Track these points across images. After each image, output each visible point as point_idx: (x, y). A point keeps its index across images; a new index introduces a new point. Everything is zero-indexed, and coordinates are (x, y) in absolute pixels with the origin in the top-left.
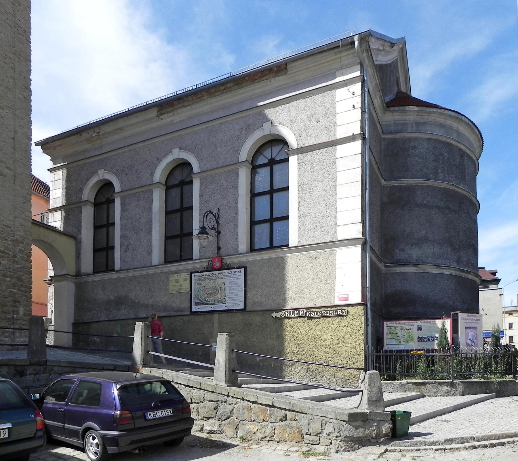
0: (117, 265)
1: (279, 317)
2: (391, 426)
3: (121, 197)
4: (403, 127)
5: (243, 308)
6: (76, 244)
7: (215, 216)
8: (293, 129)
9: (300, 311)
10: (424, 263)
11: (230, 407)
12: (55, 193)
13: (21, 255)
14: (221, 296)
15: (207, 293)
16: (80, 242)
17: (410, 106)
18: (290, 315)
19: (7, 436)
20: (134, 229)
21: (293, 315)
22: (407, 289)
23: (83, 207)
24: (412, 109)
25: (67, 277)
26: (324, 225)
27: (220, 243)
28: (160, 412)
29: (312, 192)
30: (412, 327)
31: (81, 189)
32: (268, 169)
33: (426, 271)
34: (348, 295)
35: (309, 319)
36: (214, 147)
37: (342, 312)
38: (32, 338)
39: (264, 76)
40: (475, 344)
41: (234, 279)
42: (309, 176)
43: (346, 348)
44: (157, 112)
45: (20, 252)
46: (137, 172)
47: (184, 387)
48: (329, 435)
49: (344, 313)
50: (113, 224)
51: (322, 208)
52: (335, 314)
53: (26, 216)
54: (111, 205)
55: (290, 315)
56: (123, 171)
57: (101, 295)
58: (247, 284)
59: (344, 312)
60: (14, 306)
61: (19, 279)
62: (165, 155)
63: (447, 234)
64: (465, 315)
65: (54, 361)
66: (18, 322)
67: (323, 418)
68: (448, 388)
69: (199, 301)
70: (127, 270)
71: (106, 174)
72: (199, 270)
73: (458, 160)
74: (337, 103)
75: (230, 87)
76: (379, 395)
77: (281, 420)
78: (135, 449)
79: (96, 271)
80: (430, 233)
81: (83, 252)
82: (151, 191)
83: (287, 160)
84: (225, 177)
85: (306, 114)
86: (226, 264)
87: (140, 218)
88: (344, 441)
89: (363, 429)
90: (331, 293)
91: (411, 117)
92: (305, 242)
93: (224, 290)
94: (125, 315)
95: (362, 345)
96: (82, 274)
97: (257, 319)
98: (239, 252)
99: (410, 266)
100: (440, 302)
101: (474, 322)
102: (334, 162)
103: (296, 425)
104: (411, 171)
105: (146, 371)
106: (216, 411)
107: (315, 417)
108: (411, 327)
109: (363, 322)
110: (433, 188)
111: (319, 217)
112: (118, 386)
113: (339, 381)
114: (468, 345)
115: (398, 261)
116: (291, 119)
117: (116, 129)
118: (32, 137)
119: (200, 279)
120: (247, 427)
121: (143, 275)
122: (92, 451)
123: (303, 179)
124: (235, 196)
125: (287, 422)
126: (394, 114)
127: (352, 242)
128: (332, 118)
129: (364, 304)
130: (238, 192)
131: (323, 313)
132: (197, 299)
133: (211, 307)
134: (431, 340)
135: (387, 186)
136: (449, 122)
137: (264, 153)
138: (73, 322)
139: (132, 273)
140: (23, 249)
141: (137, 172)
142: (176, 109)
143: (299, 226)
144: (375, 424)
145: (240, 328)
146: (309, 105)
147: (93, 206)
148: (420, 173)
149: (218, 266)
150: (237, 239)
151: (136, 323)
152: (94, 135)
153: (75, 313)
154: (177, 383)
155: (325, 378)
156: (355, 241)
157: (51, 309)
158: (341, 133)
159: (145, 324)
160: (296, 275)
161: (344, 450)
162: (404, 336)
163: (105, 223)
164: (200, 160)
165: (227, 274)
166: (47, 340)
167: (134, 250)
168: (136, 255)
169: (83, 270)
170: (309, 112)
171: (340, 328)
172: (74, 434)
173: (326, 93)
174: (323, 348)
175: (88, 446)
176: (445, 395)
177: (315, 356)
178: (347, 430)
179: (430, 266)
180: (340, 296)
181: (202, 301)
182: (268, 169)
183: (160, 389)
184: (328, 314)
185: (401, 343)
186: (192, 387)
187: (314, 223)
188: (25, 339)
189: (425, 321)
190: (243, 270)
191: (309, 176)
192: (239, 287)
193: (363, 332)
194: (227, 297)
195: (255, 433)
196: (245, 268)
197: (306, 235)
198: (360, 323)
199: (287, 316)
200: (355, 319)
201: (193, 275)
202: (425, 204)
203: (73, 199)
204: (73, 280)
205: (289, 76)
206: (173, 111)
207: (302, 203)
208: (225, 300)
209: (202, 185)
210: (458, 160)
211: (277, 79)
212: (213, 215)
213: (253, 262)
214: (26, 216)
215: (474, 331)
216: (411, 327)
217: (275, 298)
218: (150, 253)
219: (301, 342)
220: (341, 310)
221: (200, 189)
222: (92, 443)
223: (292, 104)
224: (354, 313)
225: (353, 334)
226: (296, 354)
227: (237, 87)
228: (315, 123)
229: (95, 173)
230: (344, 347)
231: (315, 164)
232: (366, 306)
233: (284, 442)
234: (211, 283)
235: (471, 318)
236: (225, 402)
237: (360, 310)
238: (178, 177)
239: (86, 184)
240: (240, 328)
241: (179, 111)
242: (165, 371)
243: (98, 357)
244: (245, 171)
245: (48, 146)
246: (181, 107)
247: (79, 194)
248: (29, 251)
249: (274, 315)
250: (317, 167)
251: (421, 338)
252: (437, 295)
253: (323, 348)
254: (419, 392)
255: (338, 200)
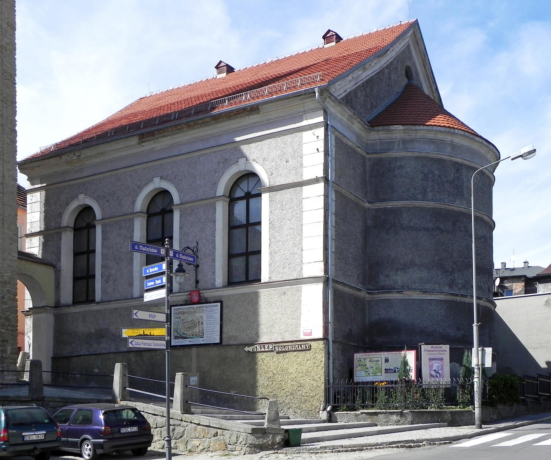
0: (98, 296)
1: (251, 351)
2: (282, 437)
3: (102, 225)
4: (388, 146)
5: (218, 341)
6: (55, 272)
7: (193, 251)
8: (265, 167)
9: (270, 345)
10: (409, 289)
11: (182, 429)
12: (32, 217)
13: (8, 295)
14: (199, 330)
15: (187, 327)
16: (59, 271)
17: (395, 125)
18: (261, 349)
19: (43, 438)
20: (115, 259)
21: (264, 349)
22: (392, 317)
23: (62, 233)
24: (397, 129)
25: (47, 309)
26: (292, 262)
27: (198, 276)
28: (129, 428)
29: (281, 230)
30: (380, 359)
31: (60, 213)
32: (244, 202)
33: (412, 298)
34: (311, 330)
35: (278, 353)
36: (193, 179)
37: (306, 347)
38: (33, 378)
39: (239, 114)
40: (440, 375)
41: (211, 313)
42: (279, 214)
43: (309, 381)
44: (138, 140)
45: (8, 292)
46: (118, 199)
47: (152, 415)
48: (240, 444)
49: (308, 348)
50: (94, 251)
51: (290, 246)
52: (300, 348)
53: (13, 257)
54: (92, 231)
55: (261, 349)
56: (104, 197)
57: (82, 328)
58: (223, 318)
59: (307, 346)
60: (3, 346)
61: (7, 319)
62: (147, 184)
63: (437, 257)
64: (429, 347)
65: (50, 397)
66: (6, 361)
67: (238, 432)
68: (398, 418)
69: (178, 335)
70: (109, 301)
71: (86, 199)
72: (179, 304)
73: (452, 175)
74: (304, 145)
75: (208, 122)
76: (276, 416)
77: (214, 436)
78: (113, 452)
79: (75, 302)
80: (417, 256)
81: (62, 281)
82: (132, 221)
83: (259, 195)
84: (203, 210)
85: (277, 153)
86: (204, 298)
87: (121, 247)
88: (249, 447)
89: (262, 439)
90: (297, 328)
91: (398, 135)
92: (275, 278)
93: (202, 324)
94: (106, 349)
95: (323, 378)
96: (62, 305)
97: (231, 353)
98: (216, 286)
99: (394, 293)
100: (427, 329)
101: (440, 353)
102: (301, 202)
103: (223, 438)
104: (397, 192)
105: (124, 403)
106: (173, 432)
107: (233, 432)
108: (379, 359)
109: (324, 356)
110: (421, 209)
111: (287, 254)
112: (103, 412)
113: (303, 413)
114: (431, 376)
115: (382, 288)
116: (264, 157)
117: (97, 154)
118: (17, 178)
119: (179, 313)
120: (193, 443)
121: (124, 307)
122: (87, 453)
123: (273, 216)
124: (213, 230)
125: (218, 437)
126: (379, 133)
127: (314, 280)
128: (299, 159)
129: (325, 339)
130: (215, 226)
131: (290, 348)
132: (176, 333)
133: (190, 341)
134: (397, 372)
135: (373, 209)
136: (440, 136)
137: (241, 186)
138: (52, 357)
139: (114, 305)
140: (10, 289)
141: (118, 199)
142: (157, 138)
143: (270, 262)
144: (271, 436)
145: (217, 362)
146: (279, 144)
147: (73, 231)
148: (406, 194)
149: (196, 299)
150: (214, 273)
151: (116, 364)
152: (75, 158)
153: (54, 347)
154: (147, 413)
155: (291, 410)
156: (317, 279)
157: (28, 342)
158: (307, 176)
159: (123, 365)
160: (267, 310)
161: (249, 453)
162: (372, 367)
163: (85, 249)
164: (180, 191)
165: (204, 308)
166: (25, 376)
167: (115, 281)
168: (117, 286)
169: (63, 301)
170: (279, 152)
171: (304, 362)
172: (74, 445)
173: (295, 134)
174: (289, 381)
175: (84, 451)
176: (395, 424)
177: (282, 389)
178: (252, 439)
179: (416, 292)
180: (305, 332)
181: (181, 335)
182: (244, 202)
183: (131, 415)
184: (294, 349)
185: (370, 375)
186: (157, 415)
187: (283, 260)
188: (12, 377)
189: (392, 353)
190: (219, 304)
191: (279, 214)
192: (215, 321)
193: (323, 366)
194: (205, 331)
195: (198, 447)
196: (221, 302)
197: (276, 271)
198: (321, 357)
199: (258, 350)
200: (317, 353)
201: (173, 308)
202: (412, 227)
203: (52, 224)
204: (52, 311)
205: (262, 115)
206: (153, 140)
207: (273, 240)
208: (202, 334)
209: (182, 217)
210: (452, 175)
211: (251, 117)
212: (191, 249)
213: (229, 296)
214: (13, 257)
215: (439, 362)
216: (379, 359)
217: (248, 333)
218: (131, 284)
219: (270, 375)
220: (305, 344)
221: (180, 221)
222: (87, 449)
223: (265, 142)
224: (316, 348)
225: (315, 367)
226: (265, 387)
227: (215, 121)
228: (285, 163)
229: (75, 197)
230: (307, 379)
231: (284, 202)
232: (328, 340)
233: (216, 451)
234: (189, 317)
235: (436, 349)
236: (180, 425)
237: (321, 344)
238: (159, 206)
239: (66, 208)
240: (217, 362)
241: (160, 140)
242: (138, 403)
243: (83, 393)
244: (222, 205)
245: (25, 166)
246: (162, 137)
247: (58, 218)
248: (15, 291)
249: (247, 349)
250: (286, 206)
251: (388, 369)
252: (424, 322)
253: (289, 381)
254: (372, 421)
255: (303, 239)
